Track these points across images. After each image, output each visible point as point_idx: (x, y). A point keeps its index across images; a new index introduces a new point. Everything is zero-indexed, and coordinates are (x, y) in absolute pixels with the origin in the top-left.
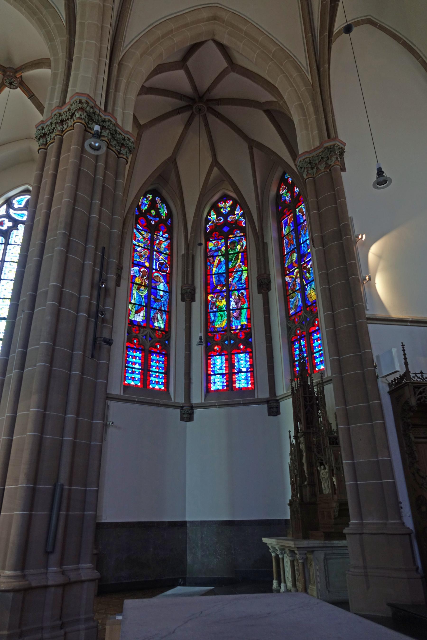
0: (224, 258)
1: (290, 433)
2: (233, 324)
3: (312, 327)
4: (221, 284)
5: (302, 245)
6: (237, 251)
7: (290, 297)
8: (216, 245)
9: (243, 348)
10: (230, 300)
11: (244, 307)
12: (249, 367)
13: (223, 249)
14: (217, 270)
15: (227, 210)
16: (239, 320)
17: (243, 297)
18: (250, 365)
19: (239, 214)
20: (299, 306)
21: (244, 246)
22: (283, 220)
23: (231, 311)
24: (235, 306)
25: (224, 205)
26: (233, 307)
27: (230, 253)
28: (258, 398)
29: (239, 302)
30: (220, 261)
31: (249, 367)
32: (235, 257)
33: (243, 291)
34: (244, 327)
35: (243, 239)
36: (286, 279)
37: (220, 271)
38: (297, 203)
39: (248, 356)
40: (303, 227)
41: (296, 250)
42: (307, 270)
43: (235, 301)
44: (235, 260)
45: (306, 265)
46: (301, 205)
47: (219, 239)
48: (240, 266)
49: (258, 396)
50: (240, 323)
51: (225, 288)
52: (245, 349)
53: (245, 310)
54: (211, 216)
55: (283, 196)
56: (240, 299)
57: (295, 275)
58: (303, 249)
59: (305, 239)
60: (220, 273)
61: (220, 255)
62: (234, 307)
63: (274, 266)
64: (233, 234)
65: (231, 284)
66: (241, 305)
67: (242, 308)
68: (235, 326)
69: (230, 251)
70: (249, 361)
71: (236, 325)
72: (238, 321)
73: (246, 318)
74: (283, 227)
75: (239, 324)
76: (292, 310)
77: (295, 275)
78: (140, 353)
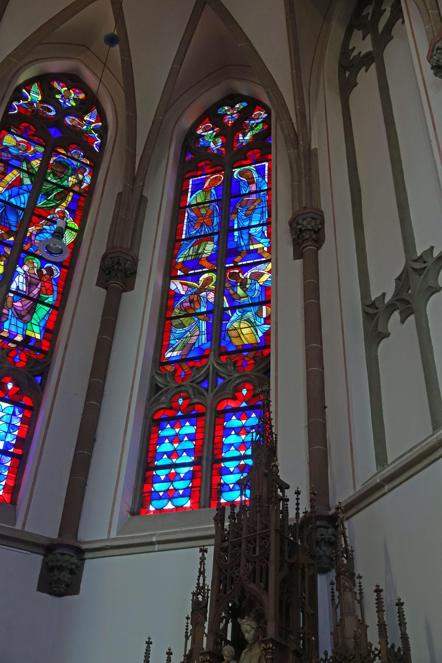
0: (31, 181)
1: (148, 647)
2: (6, 325)
3: (227, 399)
4: (5, 226)
5: (236, 234)
6: (65, 183)
7: (175, 322)
8: (21, 147)
9: (12, 389)
10: (15, 271)
11: (46, 301)
12: (14, 442)
13: (36, 163)
14: (7, 194)
15: (70, 103)
16: (25, 323)
17: (50, 280)
18: (18, 438)
19: (93, 125)
20: (196, 346)
21: (85, 185)
22: (192, 178)
23: (11, 295)
24: (23, 288)
25: (65, 91)
26: (18, 287)
27: (49, 179)
28: (22, 531)
29: (37, 285)
30: (18, 182)
31: (14, 442)
32: (58, 193)
33: (54, 267)
34: (31, 344)
35: (88, 170)
36: (172, 284)
37: (13, 201)
38: (241, 160)
39: (21, 416)
40: (244, 202)
41: (216, 238)
42: (239, 281)
43: (26, 278)
44: (55, 198)
45: (237, 271)
46: (250, 165)
47: (31, 141)
48: (63, 216)
49: (24, 525)
50: (24, 330)
51: (12, 239)
52: (17, 393)
53: (48, 309)
54: (29, 92)
55: (204, 140)
56: (40, 280)
57: (201, 283)
58: (236, 240)
59: (246, 224)
60: (11, 204)
61: (24, 171)
62: (21, 288)
63: (154, 247)
64: (67, 150)
65: (30, 238)
66: (39, 292)
67: (37, 301)
68: (10, 332)
69: (51, 175)
70: (18, 427)
71: (13, 329)
72: (20, 324)
73: (42, 324)
74: (190, 190)
75: (20, 331)
76: (173, 351)
77: (201, 283)
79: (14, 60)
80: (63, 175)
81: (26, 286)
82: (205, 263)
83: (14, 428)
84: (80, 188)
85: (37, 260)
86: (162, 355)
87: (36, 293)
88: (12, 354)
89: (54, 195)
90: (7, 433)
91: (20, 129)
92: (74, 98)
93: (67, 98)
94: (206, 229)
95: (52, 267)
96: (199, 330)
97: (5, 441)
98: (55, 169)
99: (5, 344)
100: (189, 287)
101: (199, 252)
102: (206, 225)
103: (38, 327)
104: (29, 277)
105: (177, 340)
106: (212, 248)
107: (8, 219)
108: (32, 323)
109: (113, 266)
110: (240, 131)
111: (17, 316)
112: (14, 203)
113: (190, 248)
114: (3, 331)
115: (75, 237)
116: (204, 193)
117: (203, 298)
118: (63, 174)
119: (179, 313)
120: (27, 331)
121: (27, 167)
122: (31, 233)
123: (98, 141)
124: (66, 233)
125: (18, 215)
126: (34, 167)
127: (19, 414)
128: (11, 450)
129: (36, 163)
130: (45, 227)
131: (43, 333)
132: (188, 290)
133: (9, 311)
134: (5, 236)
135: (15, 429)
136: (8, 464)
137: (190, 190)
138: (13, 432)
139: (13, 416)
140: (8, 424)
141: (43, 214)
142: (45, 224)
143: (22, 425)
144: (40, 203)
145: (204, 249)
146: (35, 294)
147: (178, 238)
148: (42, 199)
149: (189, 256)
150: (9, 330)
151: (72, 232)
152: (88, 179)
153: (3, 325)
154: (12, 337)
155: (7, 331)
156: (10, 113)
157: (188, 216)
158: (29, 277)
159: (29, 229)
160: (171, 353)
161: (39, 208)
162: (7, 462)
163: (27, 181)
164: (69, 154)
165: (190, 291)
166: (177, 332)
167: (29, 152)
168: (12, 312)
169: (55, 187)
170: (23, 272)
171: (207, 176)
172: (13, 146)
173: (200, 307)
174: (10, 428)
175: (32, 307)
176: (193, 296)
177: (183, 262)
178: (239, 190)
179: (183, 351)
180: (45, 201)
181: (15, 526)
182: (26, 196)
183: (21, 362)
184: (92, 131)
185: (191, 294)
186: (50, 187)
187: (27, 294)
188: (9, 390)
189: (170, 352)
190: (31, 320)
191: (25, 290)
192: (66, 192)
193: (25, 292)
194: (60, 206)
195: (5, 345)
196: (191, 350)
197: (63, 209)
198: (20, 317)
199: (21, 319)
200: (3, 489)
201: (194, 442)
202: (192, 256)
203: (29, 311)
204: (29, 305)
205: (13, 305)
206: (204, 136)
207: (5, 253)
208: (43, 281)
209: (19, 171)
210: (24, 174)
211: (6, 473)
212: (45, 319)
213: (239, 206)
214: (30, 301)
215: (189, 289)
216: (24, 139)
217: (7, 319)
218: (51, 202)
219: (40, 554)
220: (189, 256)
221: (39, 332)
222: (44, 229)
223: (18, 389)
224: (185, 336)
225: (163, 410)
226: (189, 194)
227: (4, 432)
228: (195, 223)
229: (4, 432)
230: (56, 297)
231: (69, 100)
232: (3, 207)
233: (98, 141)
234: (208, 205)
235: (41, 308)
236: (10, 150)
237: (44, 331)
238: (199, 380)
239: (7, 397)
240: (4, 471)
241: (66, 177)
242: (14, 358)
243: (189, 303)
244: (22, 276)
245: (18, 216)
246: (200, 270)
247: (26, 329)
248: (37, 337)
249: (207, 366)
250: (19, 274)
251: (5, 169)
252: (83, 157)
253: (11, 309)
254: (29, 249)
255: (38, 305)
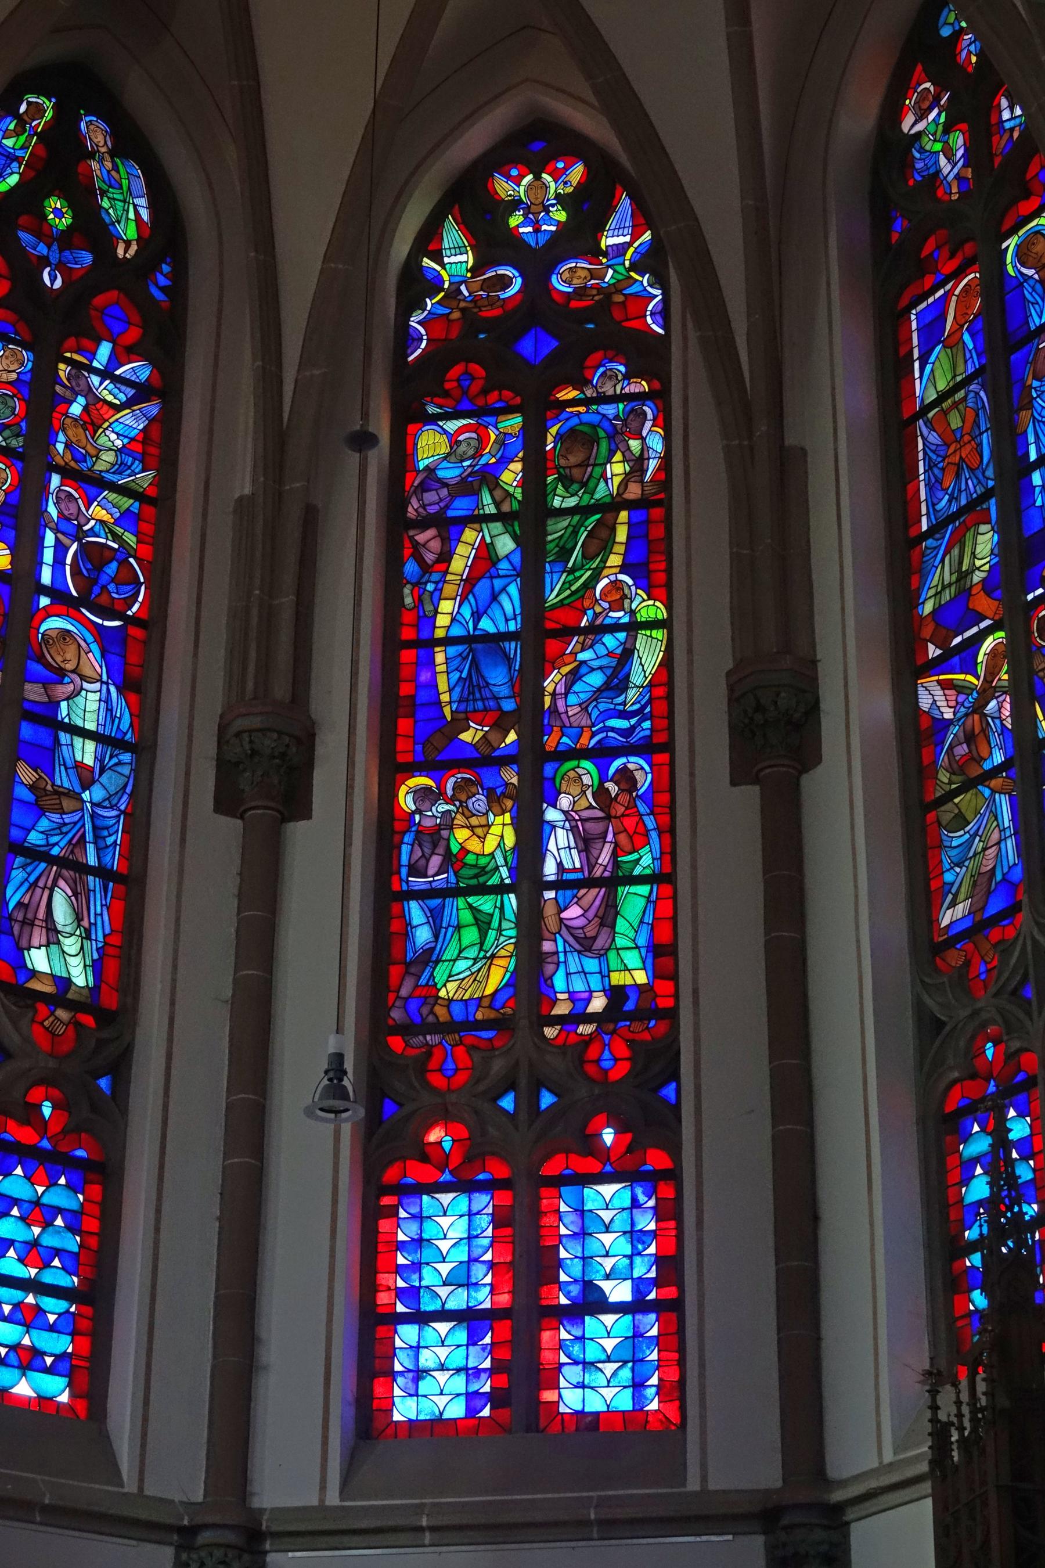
0: (515, 538)
2: (559, 982)
6: (601, 491)
7: (946, 813)
8: (463, 447)
9: (615, 1142)
12: (653, 1274)
13: (511, 476)
14: (466, 611)
16: (601, 955)
17: (631, 806)
18: (659, 1260)
20: (999, 877)
21: (653, 464)
23: (549, 895)
24: (573, 860)
26: (560, 865)
27: (557, 503)
28: (704, 1491)
30: (485, 556)
31: (653, 1274)
33: (635, 762)
34: (630, 1006)
39: (651, 1203)
43: (574, 829)
44: (587, 556)
48: (617, 597)
49: (704, 1479)
50: (604, 974)
51: (512, 737)
52: (630, 1149)
53: (644, 890)
54: (438, 258)
55: (922, 150)
56: (608, 818)
57: (981, 670)
62: (568, 865)
64: (581, 383)
65: (554, 710)
66: (615, 855)
68: (573, 996)
69: (560, 490)
70: (654, 1234)
71: (578, 985)
72: (591, 965)
73: (642, 941)
74: (916, 354)
75: (595, 982)
76: (953, 904)
77: (981, 670)
78: (72, 1187)
79: (340, 266)
80: (590, 469)
81: (579, 852)
82: (982, 603)
83: (644, 1238)
84: (642, 482)
85: (587, 764)
86: (933, 921)
87: (607, 859)
88: (592, 1053)
89: (582, 546)
90: (630, 1257)
91: (447, 394)
92: (558, 196)
93: (541, 208)
94: (970, 482)
95: (630, 766)
96: (998, 825)
97: (632, 1279)
98: (563, 462)
99: (569, 1032)
100: (959, 693)
101: (964, 569)
102: (968, 466)
103: (636, 952)
104: (579, 823)
105: (958, 870)
106: (989, 547)
107: (488, 684)
108: (618, 949)
109: (752, 719)
110: (998, 91)
111: (577, 947)
112: (492, 629)
113: (942, 561)
114: (554, 1002)
115: (665, 642)
116: (949, 351)
117: (993, 718)
118: (588, 465)
119: (950, 783)
120: (612, 974)
121: (495, 502)
122: (554, 694)
123: (656, 296)
124: (638, 646)
125: (508, 658)
126: (511, 490)
127: (646, 1199)
128: (652, 1296)
129: (513, 475)
130: (581, 656)
131: (649, 961)
132: (957, 703)
133: (555, 941)
134: (493, 738)
135: (647, 1239)
136: (654, 1332)
137: (916, 354)
138: (645, 1249)
139: (634, 1211)
140: (628, 1235)
141: (566, 618)
142: (579, 646)
143: (662, 1225)
144: (552, 590)
145: (974, 555)
146: (605, 863)
147: (913, 533)
148: (555, 577)
149: (944, 588)
150: (568, 992)
151: (654, 633)
152: (656, 443)
153: (553, 987)
154: (580, 1005)
155: (566, 996)
156: (410, 359)
157: (924, 449)
158: (579, 823)
159: (545, 684)
160: (951, 910)
161: (554, 607)
162: (649, 1327)
163: (505, 545)
164: (589, 392)
165: (962, 704)
166: (954, 844)
167: (487, 450)
168: (565, 941)
169: (577, 518)
170: (562, 817)
171: (948, 287)
172: (445, 458)
173: (991, 753)
174: (635, 1242)
175: (607, 906)
176: (970, 717)
177: (934, 612)
178: (1026, 318)
179: (975, 899)
180: (565, 575)
181: (684, 1485)
182: (513, 590)
183: (619, 1063)
184: (633, 274)
185: (966, 715)
186: (566, 528)
187: (586, 873)
188: (609, 1149)
189: (948, 908)
190: (614, 940)
191: (578, 865)
192: (609, 516)
193: (581, 870)
194: (606, 572)
195: (572, 1035)
196: (989, 893)
197: (613, 578)
198: (585, 945)
199: (590, 951)
200: (657, 1393)
201: (1031, 1162)
202: (950, 585)
203: (602, 918)
204: (597, 903)
205: (561, 920)
206: (919, 135)
207: (506, 784)
208: (615, 817)
209: (476, 526)
210: (492, 525)
211: (654, 1356)
212: (646, 921)
213: (1031, 377)
214: (597, 890)
215: (961, 698)
216: (464, 418)
217: (558, 964)
218: (577, 574)
219: (754, 1533)
220: (944, 588)
221: (641, 965)
222: (584, 662)
223: (629, 1137)
224: (971, 854)
225: (958, 1086)
226: (917, 365)
227: (625, 1256)
228: (943, 469)
229: (625, 1256)
230: (658, 846)
231: (548, 212)
232: (468, 655)
233: (656, 296)
234: (961, 394)
235: (630, 897)
236: (441, 474)
237: (650, 955)
238: (1014, 983)
239: (608, 1168)
240: (648, 1353)
241: (598, 471)
242: (598, 1061)
243: (965, 746)
244: (563, 828)
245: (509, 661)
246: (974, 630)
247: (609, 971)
248: (639, 982)
249: (1021, 938)
250: (554, 827)
251: (443, 540)
252: (627, 377)
253: (559, 933)
254: (559, 742)
255: (620, 889)
